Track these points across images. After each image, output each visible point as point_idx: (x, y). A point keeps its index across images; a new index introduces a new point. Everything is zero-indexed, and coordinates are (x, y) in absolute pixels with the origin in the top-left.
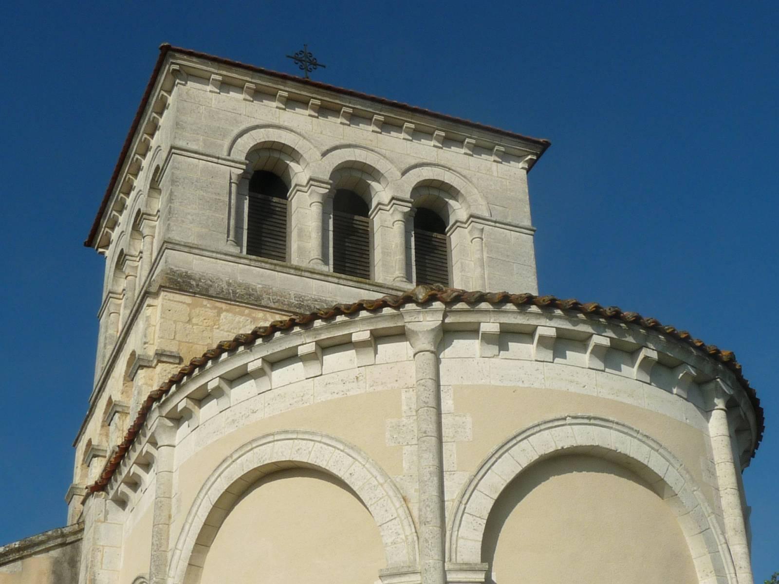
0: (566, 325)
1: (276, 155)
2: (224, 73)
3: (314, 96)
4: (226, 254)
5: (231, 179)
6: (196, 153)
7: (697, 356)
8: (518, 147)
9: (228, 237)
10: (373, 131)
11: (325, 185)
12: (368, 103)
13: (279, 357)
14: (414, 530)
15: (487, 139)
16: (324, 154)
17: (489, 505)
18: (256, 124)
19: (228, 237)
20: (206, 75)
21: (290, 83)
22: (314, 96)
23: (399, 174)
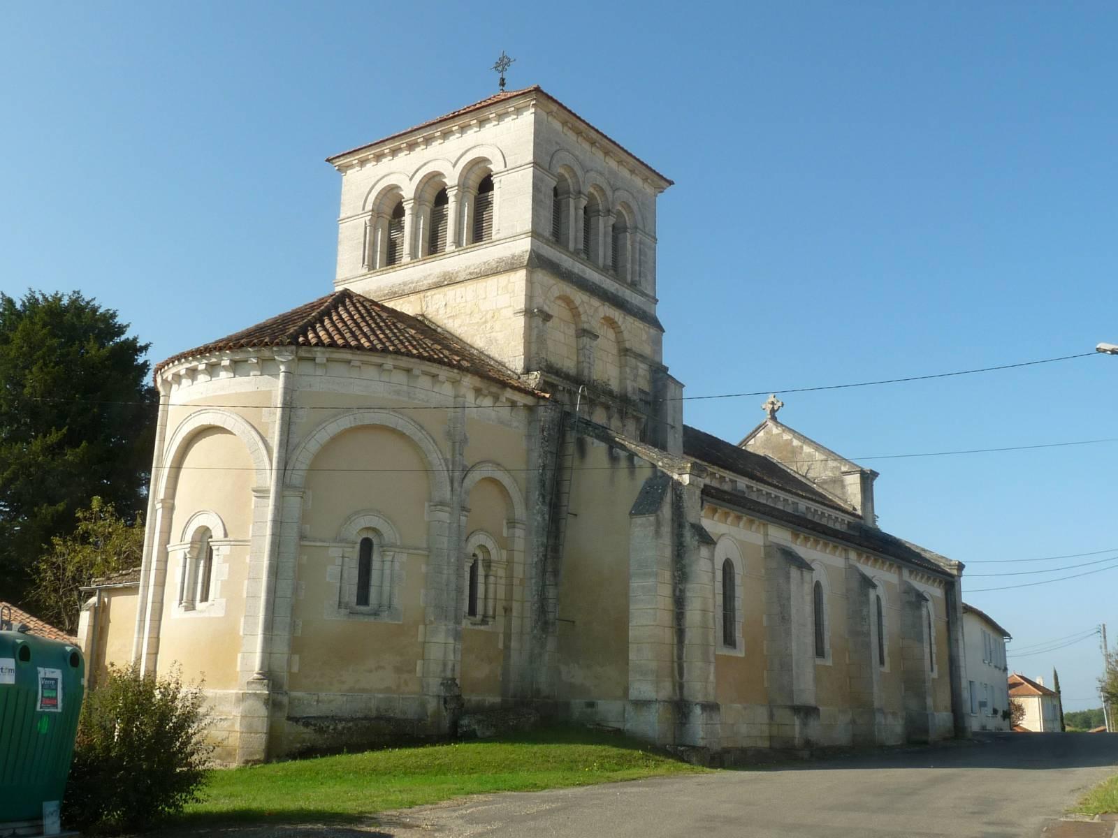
0: (188, 365)
1: (481, 165)
2: (373, 152)
3: (401, 142)
4: (360, 277)
5: (366, 224)
6: (348, 218)
7: (254, 351)
8: (521, 102)
9: (363, 263)
10: (440, 144)
11: (410, 202)
12: (348, 156)
13: (592, 237)
14: (288, 472)
15: (500, 109)
16: (411, 179)
17: (367, 422)
18: (376, 180)
19: (363, 263)
20: (450, 130)
21: (386, 143)
22: (401, 142)
23: (452, 168)
